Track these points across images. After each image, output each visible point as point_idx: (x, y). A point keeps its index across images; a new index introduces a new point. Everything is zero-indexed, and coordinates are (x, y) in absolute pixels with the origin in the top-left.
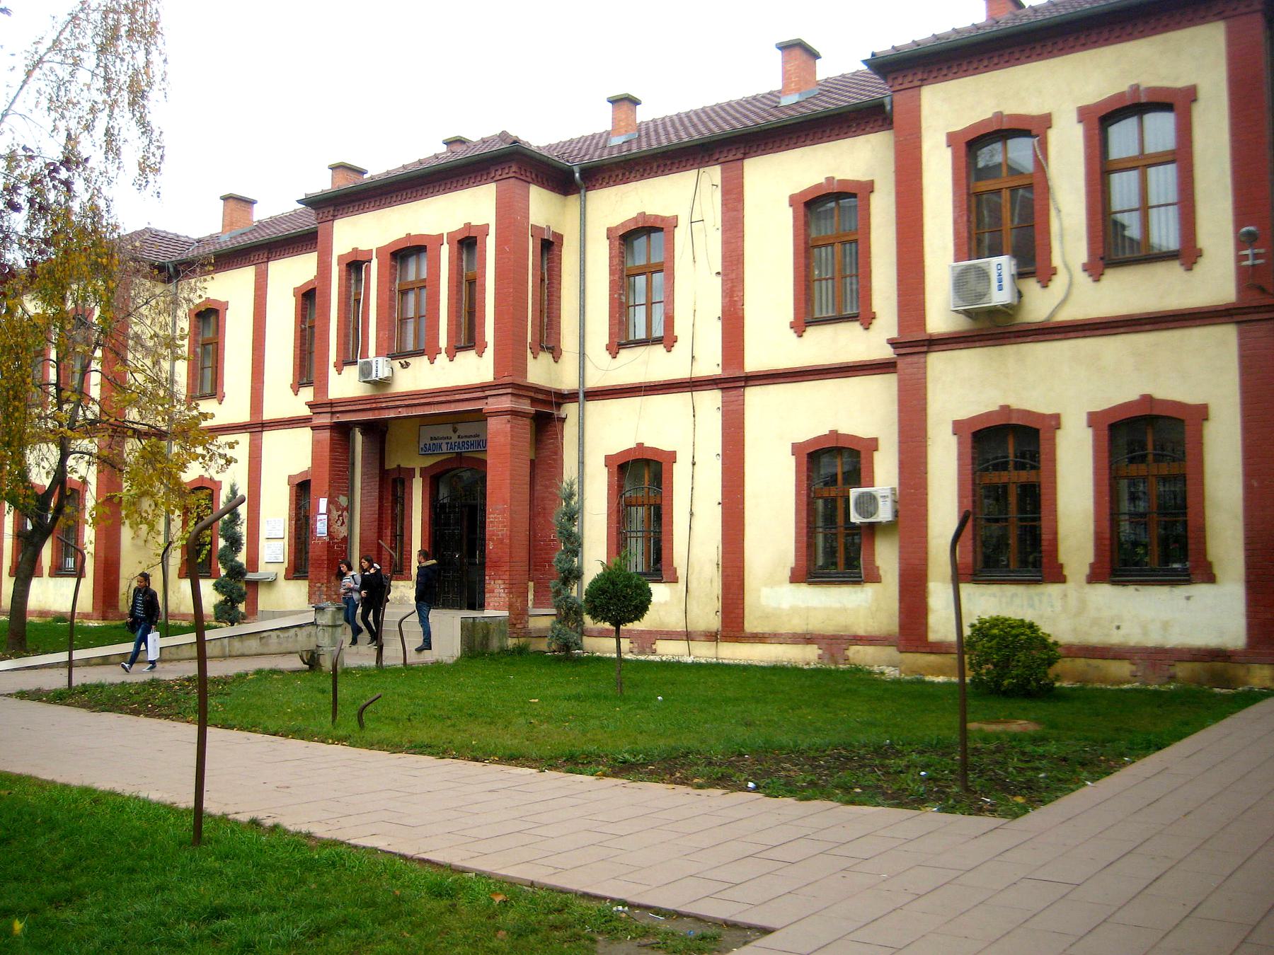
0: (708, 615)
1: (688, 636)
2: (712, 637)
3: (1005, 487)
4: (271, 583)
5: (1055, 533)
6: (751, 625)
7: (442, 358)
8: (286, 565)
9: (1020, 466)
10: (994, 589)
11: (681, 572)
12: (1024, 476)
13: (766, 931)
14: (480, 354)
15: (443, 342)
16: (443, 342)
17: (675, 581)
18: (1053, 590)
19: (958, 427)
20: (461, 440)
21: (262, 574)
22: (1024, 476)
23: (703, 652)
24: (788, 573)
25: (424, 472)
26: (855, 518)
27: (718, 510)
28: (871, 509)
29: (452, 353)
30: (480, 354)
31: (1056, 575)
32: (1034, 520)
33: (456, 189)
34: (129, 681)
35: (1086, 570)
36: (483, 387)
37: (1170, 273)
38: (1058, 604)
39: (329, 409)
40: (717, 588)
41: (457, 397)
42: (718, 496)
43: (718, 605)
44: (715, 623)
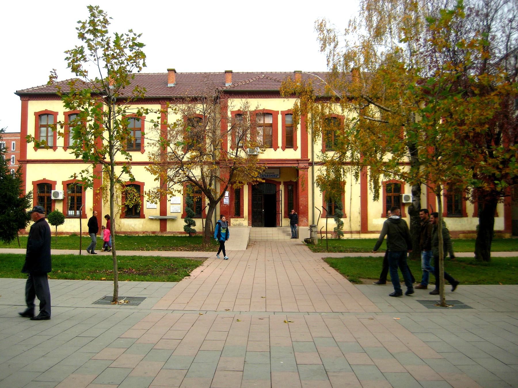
0: (356, 226)
1: (351, 232)
2: (358, 232)
3: (44, 197)
4: (173, 220)
5: (465, 206)
6: (370, 229)
7: (280, 150)
8: (182, 213)
9: (77, 192)
10: (452, 219)
11: (348, 214)
12: (78, 195)
13: (96, 303)
14: (295, 150)
15: (280, 144)
16: (280, 144)
17: (346, 217)
18: (465, 219)
19: (33, 183)
20: (267, 174)
21: (168, 217)
22: (78, 195)
23: (356, 236)
24: (380, 215)
25: (285, 184)
26: (404, 201)
27: (359, 198)
28: (408, 199)
29: (283, 149)
30: (295, 150)
31: (466, 215)
32: (200, 204)
33: (44, 100)
34: (150, 251)
35: (472, 214)
36: (298, 160)
37: (51, 151)
38: (466, 222)
39: (297, 162)
40: (359, 219)
41: (287, 162)
42: (359, 194)
43: (360, 224)
44: (359, 228)
